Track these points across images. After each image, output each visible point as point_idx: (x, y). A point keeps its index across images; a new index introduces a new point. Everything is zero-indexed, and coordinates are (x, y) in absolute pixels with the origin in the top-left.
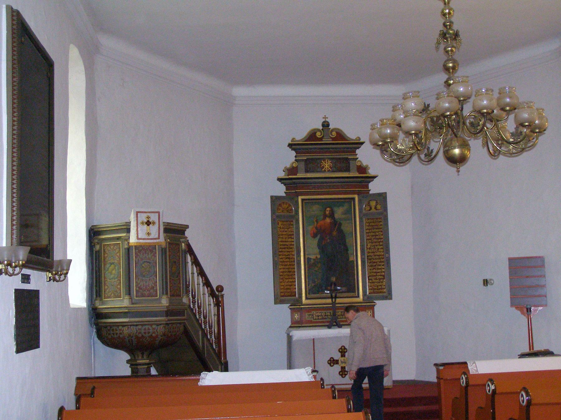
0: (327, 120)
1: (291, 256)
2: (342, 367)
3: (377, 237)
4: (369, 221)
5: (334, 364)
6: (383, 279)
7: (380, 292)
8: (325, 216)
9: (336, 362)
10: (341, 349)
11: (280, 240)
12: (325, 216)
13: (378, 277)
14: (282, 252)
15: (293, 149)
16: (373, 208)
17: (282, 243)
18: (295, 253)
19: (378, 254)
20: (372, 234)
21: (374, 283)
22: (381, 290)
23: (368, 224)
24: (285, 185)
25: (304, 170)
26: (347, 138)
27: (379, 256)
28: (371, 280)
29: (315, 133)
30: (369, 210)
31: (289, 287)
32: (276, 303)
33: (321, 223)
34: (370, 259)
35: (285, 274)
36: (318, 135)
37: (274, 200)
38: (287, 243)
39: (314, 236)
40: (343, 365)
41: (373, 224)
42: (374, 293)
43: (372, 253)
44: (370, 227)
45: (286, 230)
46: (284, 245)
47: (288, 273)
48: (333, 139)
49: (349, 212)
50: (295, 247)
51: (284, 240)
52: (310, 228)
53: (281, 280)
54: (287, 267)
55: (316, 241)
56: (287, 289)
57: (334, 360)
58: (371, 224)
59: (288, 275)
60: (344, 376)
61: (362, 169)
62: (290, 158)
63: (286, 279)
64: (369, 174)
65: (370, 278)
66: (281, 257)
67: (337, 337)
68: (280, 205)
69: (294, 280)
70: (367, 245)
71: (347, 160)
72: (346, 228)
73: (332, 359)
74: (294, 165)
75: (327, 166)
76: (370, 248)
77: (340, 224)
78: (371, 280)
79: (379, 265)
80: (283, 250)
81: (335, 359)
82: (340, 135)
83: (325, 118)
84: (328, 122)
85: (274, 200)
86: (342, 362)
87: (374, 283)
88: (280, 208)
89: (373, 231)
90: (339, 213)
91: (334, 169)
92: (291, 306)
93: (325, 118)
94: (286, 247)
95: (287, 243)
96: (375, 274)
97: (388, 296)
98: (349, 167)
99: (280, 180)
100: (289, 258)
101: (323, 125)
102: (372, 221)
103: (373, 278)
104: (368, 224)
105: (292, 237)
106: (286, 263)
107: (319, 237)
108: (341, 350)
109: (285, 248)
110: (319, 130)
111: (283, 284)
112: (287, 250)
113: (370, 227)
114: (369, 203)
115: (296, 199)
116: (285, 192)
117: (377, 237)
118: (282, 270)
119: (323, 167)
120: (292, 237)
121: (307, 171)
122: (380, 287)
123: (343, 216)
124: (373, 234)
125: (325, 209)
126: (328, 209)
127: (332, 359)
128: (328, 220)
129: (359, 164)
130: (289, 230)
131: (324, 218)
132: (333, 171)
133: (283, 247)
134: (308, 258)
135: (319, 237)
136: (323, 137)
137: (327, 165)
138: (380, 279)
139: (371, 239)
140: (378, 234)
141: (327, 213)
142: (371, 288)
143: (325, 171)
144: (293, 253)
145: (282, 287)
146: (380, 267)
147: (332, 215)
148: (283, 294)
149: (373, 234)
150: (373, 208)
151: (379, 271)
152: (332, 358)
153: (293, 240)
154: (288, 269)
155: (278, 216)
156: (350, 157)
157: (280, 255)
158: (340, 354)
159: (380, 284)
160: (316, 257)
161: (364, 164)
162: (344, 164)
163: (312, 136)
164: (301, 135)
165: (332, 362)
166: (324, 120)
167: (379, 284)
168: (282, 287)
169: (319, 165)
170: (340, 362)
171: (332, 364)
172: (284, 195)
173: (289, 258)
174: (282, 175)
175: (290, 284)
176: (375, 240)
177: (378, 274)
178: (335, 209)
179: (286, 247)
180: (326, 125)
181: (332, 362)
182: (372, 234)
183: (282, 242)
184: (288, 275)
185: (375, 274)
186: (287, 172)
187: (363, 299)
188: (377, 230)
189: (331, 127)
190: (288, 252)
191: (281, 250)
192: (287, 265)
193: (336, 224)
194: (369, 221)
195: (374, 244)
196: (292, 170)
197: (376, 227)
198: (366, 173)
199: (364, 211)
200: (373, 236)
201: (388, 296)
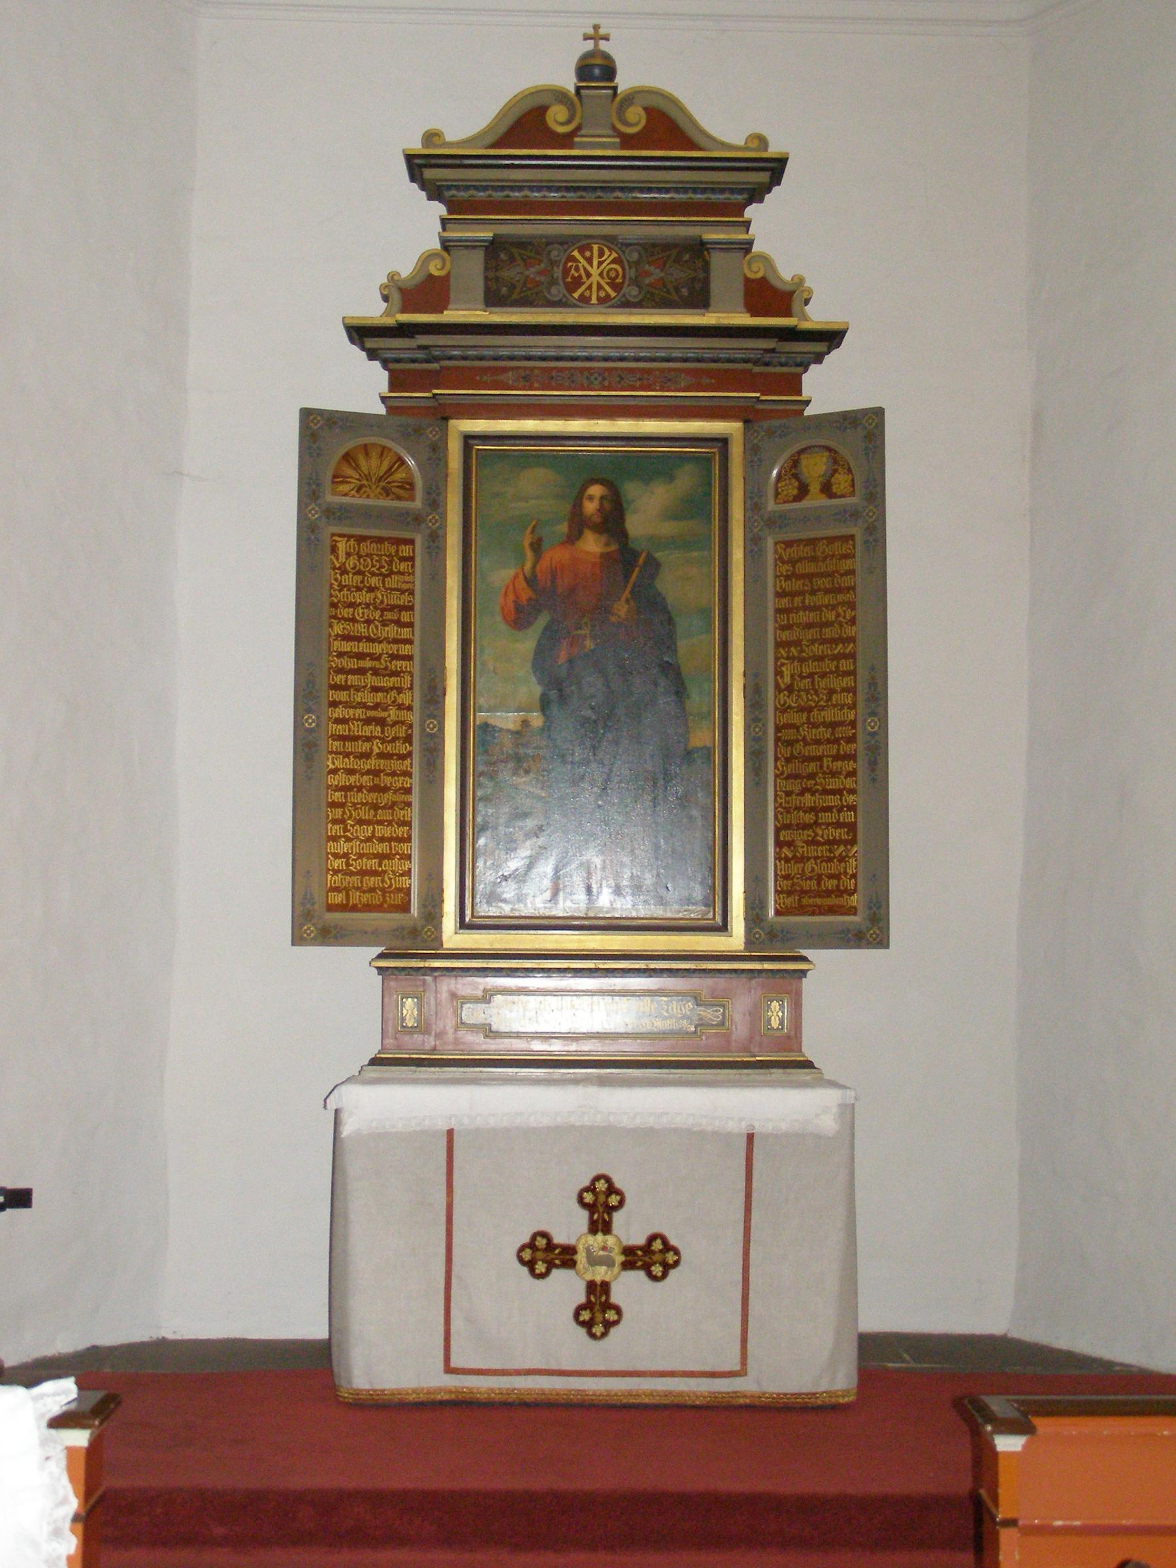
0: (603, 46)
1: (393, 714)
2: (591, 1286)
3: (828, 633)
4: (794, 552)
5: (551, 1266)
6: (853, 842)
7: (831, 910)
8: (578, 524)
9: (565, 1257)
10: (591, 1189)
11: (338, 629)
12: (578, 524)
13: (823, 834)
14: (346, 688)
15: (435, 192)
16: (815, 488)
17: (347, 647)
18: (415, 698)
19: (829, 715)
20: (804, 617)
21: (802, 859)
22: (832, 901)
23: (785, 569)
24: (385, 364)
25: (480, 293)
26: (691, 133)
27: (833, 725)
28: (790, 844)
29: (542, 110)
30: (798, 498)
31: (372, 864)
32: (298, 939)
33: (556, 555)
34: (790, 743)
35: (360, 797)
36: (557, 118)
37: (319, 428)
38: (377, 649)
39: (519, 619)
40: (600, 1274)
41: (810, 568)
42: (801, 910)
43: (801, 709)
44: (797, 585)
45: (374, 581)
46: (361, 656)
47: (372, 797)
48: (627, 141)
49: (703, 508)
50: (416, 667)
51: (361, 629)
52: (501, 575)
53: (337, 829)
54: (372, 763)
55: (526, 643)
56: (363, 873)
57: (551, 1246)
58: (801, 568)
59: (375, 807)
60: (598, 1329)
61: (768, 295)
62: (414, 229)
63: (361, 822)
64: (805, 318)
65: (785, 835)
66: (339, 712)
67: (572, 1128)
68: (348, 457)
69: (401, 831)
70: (778, 673)
71: (700, 248)
72: (679, 583)
73: (541, 1242)
74: (435, 269)
75: (595, 278)
76: (790, 689)
77: (653, 566)
78: (790, 844)
79: (834, 774)
80: (353, 679)
81: (559, 1239)
82: (665, 125)
83: (596, 36)
84: (607, 57)
85: (319, 428)
86: (593, 1261)
87: (802, 859)
88: (349, 472)
89: (809, 600)
90: (648, 511)
91: (632, 292)
92: (381, 956)
93: (596, 36)
94: (368, 664)
95: (377, 649)
96: (809, 818)
97: (872, 932)
98: (706, 282)
99: (359, 333)
100: (381, 722)
101: (584, 70)
102: (807, 551)
103: (800, 837)
104: (785, 569)
105: (405, 617)
106: (365, 747)
107: (542, 621)
108: (589, 1198)
109: (362, 671)
110: (560, 96)
111: (343, 847)
112: (371, 680)
113: (797, 585)
114: (795, 463)
115: (431, 434)
116: (384, 399)
117: (828, 633)
118: (341, 779)
119: (577, 282)
120: (405, 617)
121: (493, 299)
122: (831, 884)
123: (668, 528)
124: (812, 616)
125: (583, 489)
126: (596, 490)
127: (541, 1242)
128: (592, 545)
129: (756, 272)
130: (392, 582)
131: (573, 537)
132: (626, 304)
133: (353, 664)
134: (485, 727)
135: (542, 621)
136: (579, 128)
137: (596, 269)
138: (831, 842)
139: (798, 643)
140: (831, 616)
141: (590, 507)
142: (786, 884)
143: (585, 300)
144: (405, 699)
145: (338, 863)
146: (833, 784)
147: (612, 521)
148: (338, 898)
149: (812, 616)
150: (815, 488)
151: (832, 801)
152: (544, 1235)
153: (405, 633)
154: (375, 773)
155: (330, 513)
156: (711, 235)
157: (334, 704)
158: (584, 1215)
159: (834, 867)
160: (525, 723)
161: (786, 272)
162: (682, 272)
163: (527, 124)
164: (467, 116)
165: (544, 1255)
166: (589, 45)
167: (825, 869)
168: (338, 863)
169: (558, 272)
170: (581, 1257)
171: (540, 1267)
172: (381, 410)
173: (381, 722)
174: (373, 309)
175: (381, 848)
176: (817, 649)
177: (825, 817)
178: (631, 489)
179: (368, 664)
180: (596, 69)
181: (544, 1255)
182: (804, 617)
183: (347, 638)
184: (375, 807)
185: (809, 818)
186: (396, 297)
187: (749, 942)
188: (827, 599)
189: (625, 81)
190: (376, 689)
191: (339, 679)
192: (366, 756)
193: (628, 561)
194: (794, 552)
195: (810, 667)
196: (424, 291)
197: (824, 583)
198: (788, 313)
199: (771, 506)
200: (810, 626)
201: (872, 932)
